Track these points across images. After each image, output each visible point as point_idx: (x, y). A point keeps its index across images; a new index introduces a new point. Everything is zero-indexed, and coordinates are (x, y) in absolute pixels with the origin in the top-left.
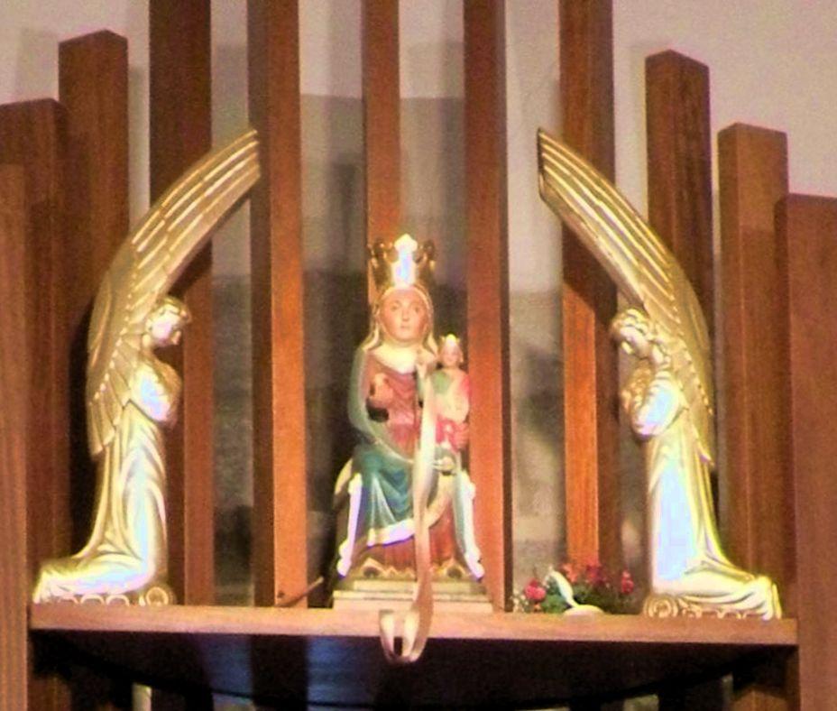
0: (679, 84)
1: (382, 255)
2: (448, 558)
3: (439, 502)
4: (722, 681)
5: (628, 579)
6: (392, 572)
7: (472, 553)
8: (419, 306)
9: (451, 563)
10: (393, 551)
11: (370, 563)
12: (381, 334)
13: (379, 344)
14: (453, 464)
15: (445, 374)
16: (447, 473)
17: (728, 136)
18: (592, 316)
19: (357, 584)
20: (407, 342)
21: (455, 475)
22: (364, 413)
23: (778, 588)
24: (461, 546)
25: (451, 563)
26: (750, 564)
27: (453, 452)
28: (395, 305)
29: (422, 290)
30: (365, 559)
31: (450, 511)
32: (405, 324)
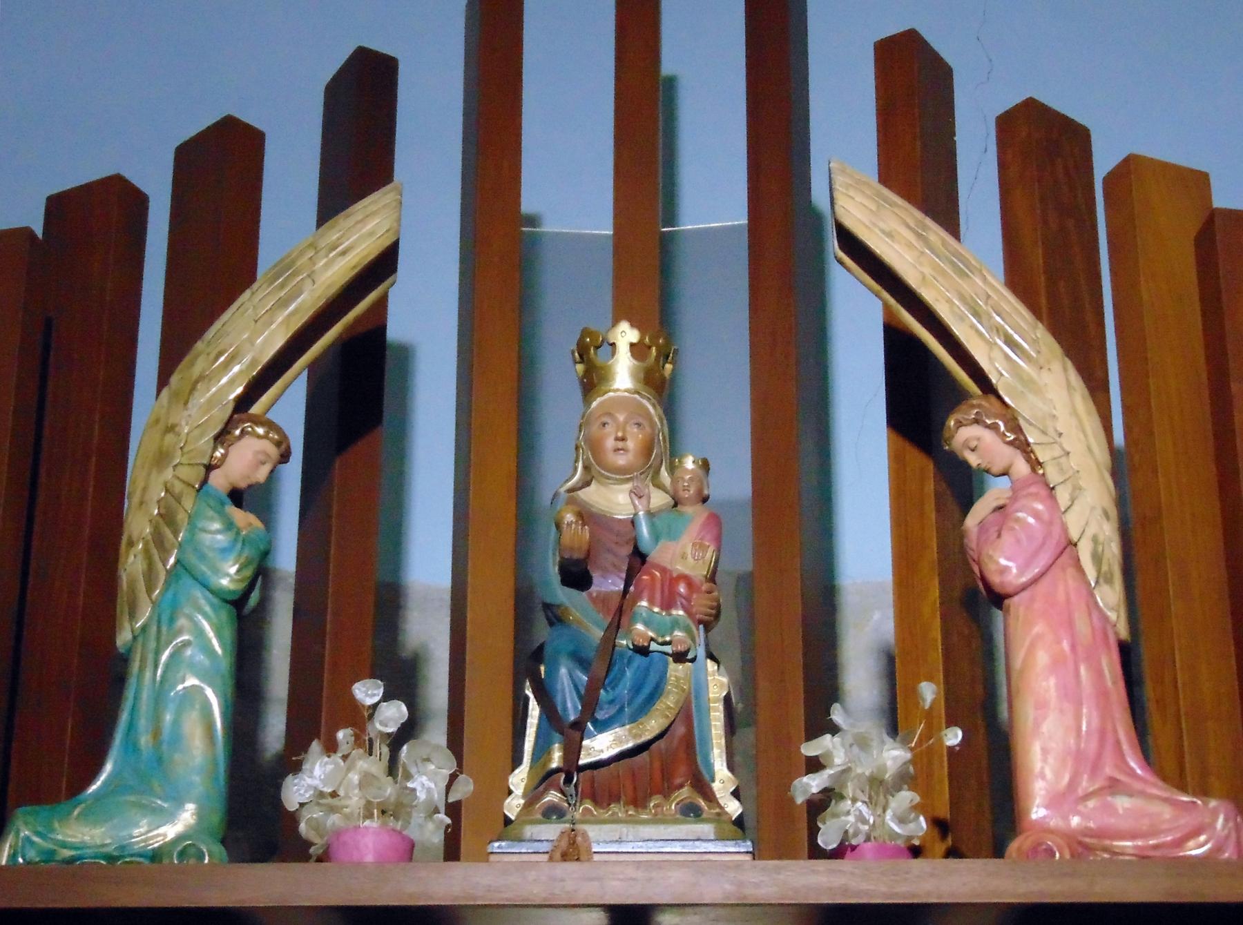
0: (1043, 144)
1: (681, 457)
2: (681, 786)
3: (669, 702)
4: (1032, 821)
5: (218, 532)
6: (586, 809)
7: (722, 779)
8: (641, 420)
9: (685, 793)
10: (592, 781)
11: (553, 797)
12: (586, 468)
13: (587, 484)
14: (689, 642)
15: (681, 514)
16: (680, 657)
17: (1129, 168)
18: (931, 466)
19: (529, 831)
20: (623, 474)
21: (693, 660)
22: (554, 571)
23: (297, 827)
24: (704, 772)
25: (685, 793)
26: (1190, 791)
27: (689, 622)
28: (605, 419)
29: (649, 399)
30: (546, 791)
31: (687, 715)
32: (620, 445)
